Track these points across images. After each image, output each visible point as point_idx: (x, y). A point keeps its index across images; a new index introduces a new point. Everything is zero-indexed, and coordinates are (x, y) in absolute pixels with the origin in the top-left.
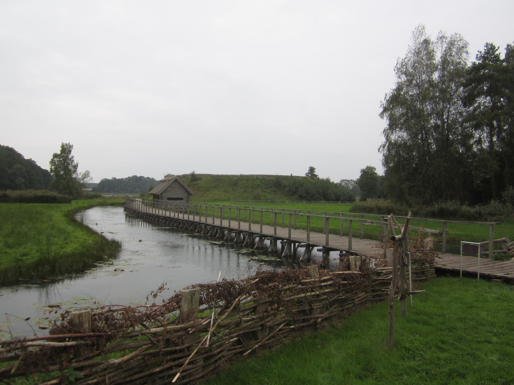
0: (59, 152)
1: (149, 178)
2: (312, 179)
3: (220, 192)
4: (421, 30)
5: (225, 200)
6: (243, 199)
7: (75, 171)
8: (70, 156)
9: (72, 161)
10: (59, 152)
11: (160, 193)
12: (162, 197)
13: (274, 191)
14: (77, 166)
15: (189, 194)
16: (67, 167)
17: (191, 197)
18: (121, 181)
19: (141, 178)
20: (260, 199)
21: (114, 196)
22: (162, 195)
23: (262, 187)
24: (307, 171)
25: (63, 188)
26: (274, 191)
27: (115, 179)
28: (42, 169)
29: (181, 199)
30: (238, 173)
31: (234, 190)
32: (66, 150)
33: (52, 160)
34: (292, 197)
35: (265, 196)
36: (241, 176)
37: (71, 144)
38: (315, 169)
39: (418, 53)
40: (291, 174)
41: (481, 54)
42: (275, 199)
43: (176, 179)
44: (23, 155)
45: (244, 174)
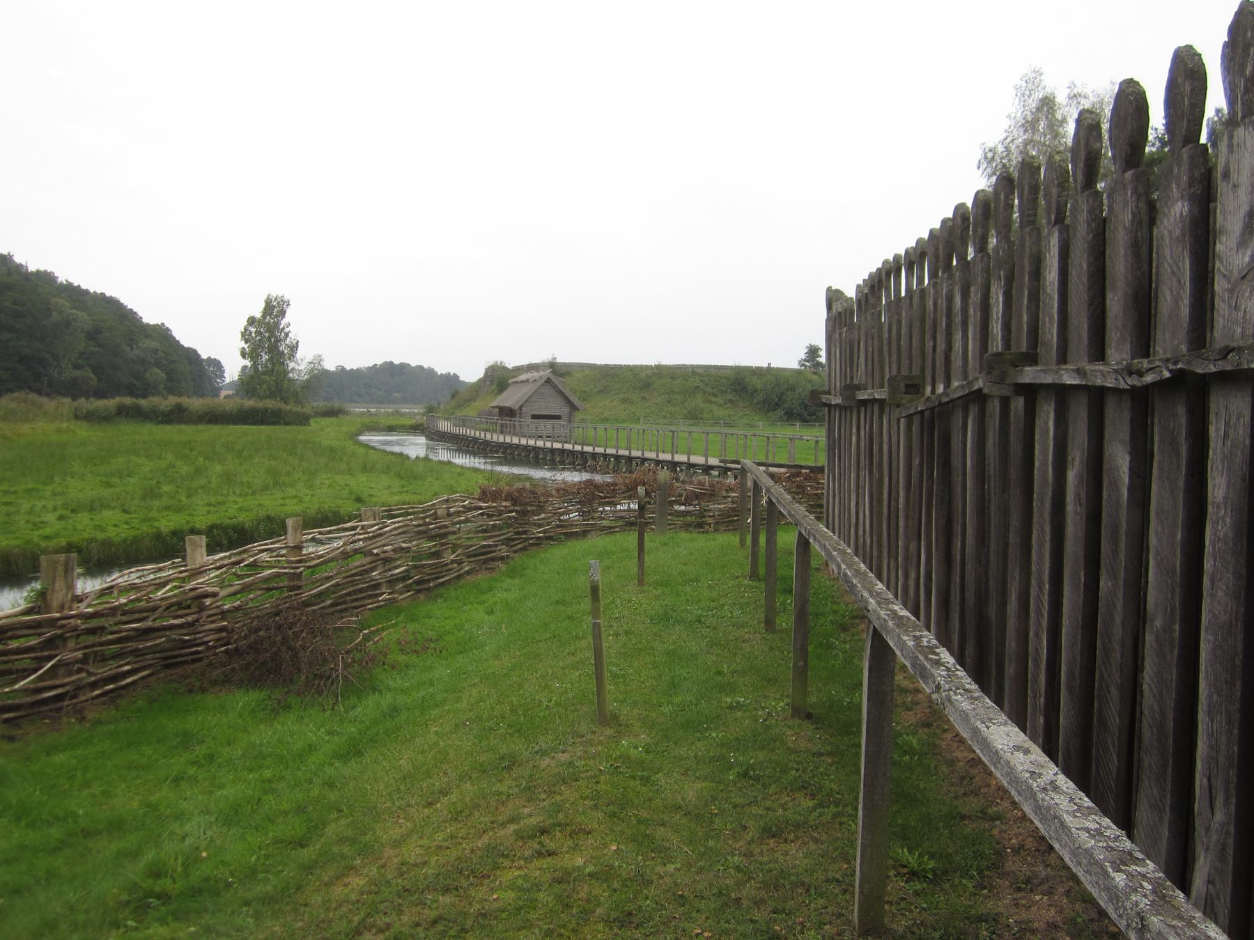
0: (258, 315)
1: (421, 367)
2: (815, 373)
3: (613, 404)
4: (1033, 80)
5: (625, 420)
6: (664, 417)
7: (292, 355)
8: (284, 322)
9: (287, 335)
10: (258, 315)
11: (518, 406)
12: (520, 414)
13: (731, 401)
14: (297, 346)
15: (574, 408)
16: (277, 347)
17: (578, 416)
18: (356, 375)
19: (404, 367)
20: (701, 419)
21: (368, 411)
22: (521, 410)
23: (704, 392)
24: (802, 354)
25: (268, 393)
26: (731, 401)
27: (343, 369)
28: (182, 346)
29: (558, 417)
30: (652, 362)
31: (644, 398)
32: (275, 309)
33: (246, 329)
34: (771, 413)
35: (711, 411)
36: (659, 367)
37: (286, 298)
38: (833, 297)
39: (1030, 125)
40: (769, 364)
41: (1157, 133)
42: (733, 418)
43: (549, 378)
44: (140, 314)
45: (664, 363)
